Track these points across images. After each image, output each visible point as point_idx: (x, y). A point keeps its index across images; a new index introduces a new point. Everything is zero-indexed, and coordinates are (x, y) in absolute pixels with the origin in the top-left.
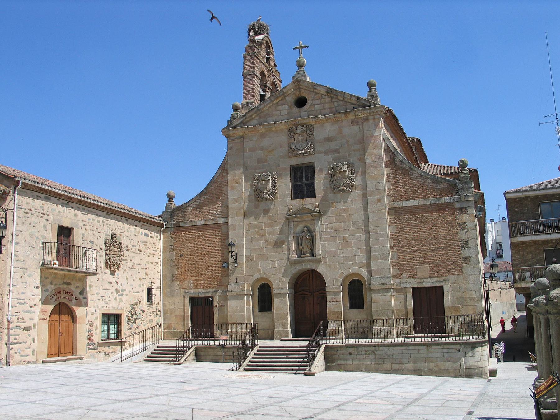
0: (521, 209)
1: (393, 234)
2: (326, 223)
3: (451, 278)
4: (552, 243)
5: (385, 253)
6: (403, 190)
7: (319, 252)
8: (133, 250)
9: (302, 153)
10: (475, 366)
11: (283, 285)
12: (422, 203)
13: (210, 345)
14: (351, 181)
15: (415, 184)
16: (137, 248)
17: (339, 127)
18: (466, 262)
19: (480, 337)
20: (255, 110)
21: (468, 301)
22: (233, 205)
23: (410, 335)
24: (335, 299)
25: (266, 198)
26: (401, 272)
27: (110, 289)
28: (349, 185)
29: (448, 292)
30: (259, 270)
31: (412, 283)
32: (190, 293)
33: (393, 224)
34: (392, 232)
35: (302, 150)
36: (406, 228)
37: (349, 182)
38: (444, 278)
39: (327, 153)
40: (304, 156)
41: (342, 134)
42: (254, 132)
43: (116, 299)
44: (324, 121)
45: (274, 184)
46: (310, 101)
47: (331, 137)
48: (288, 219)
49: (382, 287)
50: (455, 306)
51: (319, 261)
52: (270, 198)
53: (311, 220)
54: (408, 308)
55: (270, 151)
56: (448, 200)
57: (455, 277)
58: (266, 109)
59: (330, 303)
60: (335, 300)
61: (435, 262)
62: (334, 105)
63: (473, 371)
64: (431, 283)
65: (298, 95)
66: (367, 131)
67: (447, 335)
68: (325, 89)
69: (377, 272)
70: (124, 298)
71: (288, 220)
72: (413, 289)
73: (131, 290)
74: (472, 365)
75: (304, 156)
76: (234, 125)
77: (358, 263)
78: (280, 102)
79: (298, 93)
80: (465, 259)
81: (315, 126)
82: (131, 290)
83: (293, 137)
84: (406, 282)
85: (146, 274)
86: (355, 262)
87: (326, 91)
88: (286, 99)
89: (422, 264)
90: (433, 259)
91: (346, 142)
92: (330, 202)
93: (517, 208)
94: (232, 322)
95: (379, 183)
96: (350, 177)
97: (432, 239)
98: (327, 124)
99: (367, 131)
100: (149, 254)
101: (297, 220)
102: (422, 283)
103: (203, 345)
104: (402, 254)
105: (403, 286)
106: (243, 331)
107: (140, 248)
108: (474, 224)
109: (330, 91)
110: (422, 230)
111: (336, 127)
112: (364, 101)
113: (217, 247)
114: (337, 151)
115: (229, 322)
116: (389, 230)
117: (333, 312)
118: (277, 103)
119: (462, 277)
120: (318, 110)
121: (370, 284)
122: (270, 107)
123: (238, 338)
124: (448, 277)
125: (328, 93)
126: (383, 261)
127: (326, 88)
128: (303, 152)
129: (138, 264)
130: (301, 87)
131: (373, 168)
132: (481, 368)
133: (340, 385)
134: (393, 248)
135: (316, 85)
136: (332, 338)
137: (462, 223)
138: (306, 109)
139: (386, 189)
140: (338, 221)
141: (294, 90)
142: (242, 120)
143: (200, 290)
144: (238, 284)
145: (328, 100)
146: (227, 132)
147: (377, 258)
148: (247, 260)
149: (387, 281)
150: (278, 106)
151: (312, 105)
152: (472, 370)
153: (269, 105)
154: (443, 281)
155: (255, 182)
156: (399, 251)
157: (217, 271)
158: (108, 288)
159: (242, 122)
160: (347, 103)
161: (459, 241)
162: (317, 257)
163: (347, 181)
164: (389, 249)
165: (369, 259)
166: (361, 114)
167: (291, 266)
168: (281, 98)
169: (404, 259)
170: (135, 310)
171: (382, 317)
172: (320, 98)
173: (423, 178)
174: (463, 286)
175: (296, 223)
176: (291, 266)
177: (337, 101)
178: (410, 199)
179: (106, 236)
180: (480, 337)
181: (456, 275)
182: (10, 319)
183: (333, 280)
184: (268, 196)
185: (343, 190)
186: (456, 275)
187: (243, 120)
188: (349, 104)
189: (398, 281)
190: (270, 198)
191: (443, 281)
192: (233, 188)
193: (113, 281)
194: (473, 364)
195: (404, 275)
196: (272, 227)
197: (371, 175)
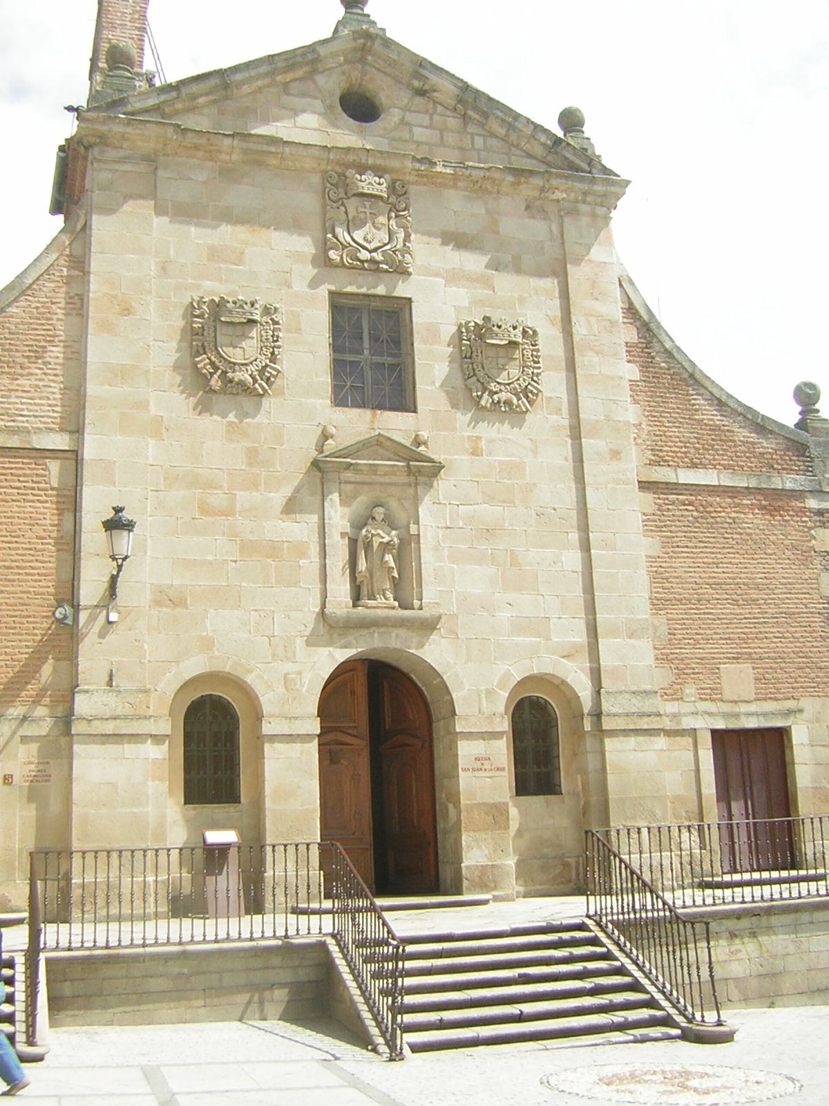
1: (653, 562)
2: (455, 503)
5: (639, 617)
7: (432, 596)
9: (372, 261)
11: (300, 704)
12: (726, 480)
13: (772, 900)
14: (533, 380)
15: (706, 425)
17: (487, 211)
20: (215, 81)
22: (107, 387)
23: (710, 879)
24: (486, 760)
25: (241, 383)
26: (680, 681)
28: (525, 391)
30: (207, 644)
33: (652, 531)
34: (650, 557)
35: (375, 250)
36: (687, 547)
37: (524, 380)
38: (791, 704)
40: (378, 270)
41: (497, 233)
42: (200, 154)
44: (447, 182)
45: (274, 341)
46: (396, 110)
47: (465, 234)
48: (320, 469)
49: (635, 724)
50: (821, 788)
51: (428, 626)
52: (257, 386)
53: (404, 484)
54: (704, 791)
56: (790, 485)
58: (246, 89)
59: (469, 773)
60: (487, 765)
62: (473, 143)
64: (761, 718)
65: (354, 81)
66: (576, 243)
67: (717, 882)
68: (455, 86)
71: (319, 474)
72: (715, 733)
75: (378, 270)
76: (129, 108)
77: (557, 642)
78: (295, 87)
79: (356, 75)
81: (413, 189)
83: (343, 204)
84: (693, 710)
86: (548, 639)
87: (457, 91)
88: (315, 82)
91: (510, 259)
94: (87, 847)
95: (615, 402)
96: (528, 367)
97: (757, 587)
98: (452, 192)
99: (576, 243)
101: (353, 480)
102: (737, 716)
103: (95, 947)
104: (679, 624)
105: (688, 723)
106: (137, 882)
109: (469, 98)
110: (730, 558)
111: (479, 209)
112: (575, 154)
113: (21, 540)
115: (76, 845)
116: (644, 546)
117: (479, 804)
118: (286, 85)
120: (426, 144)
121: (597, 715)
122: (260, 88)
123: (114, 911)
125: (460, 101)
126: (633, 641)
127: (461, 85)
128: (378, 256)
130: (369, 58)
131: (594, 355)
135: (428, 66)
136: (306, 906)
137: (825, 552)
138: (385, 129)
141: (347, 61)
142: (163, 98)
144: (119, 691)
145: (453, 122)
146: (104, 123)
147: (615, 633)
150: (289, 94)
151: (403, 122)
153: (260, 83)
154: (790, 712)
155: (199, 323)
156: (671, 613)
157: (20, 634)
159: (156, 109)
160: (513, 149)
161: (821, 601)
162: (425, 613)
163: (518, 379)
165: (593, 630)
166: (562, 190)
167: (331, 636)
168: (300, 73)
169: (684, 639)
171: (637, 822)
172: (431, 111)
173: (726, 411)
175: (349, 487)
176: (331, 636)
177: (484, 136)
178: (694, 466)
181: (819, 696)
182: (30, 763)
183: (479, 695)
184: (250, 380)
185: (508, 403)
186: (819, 696)
187: (163, 102)
188: (518, 152)
190: (257, 386)
191: (790, 712)
192: (107, 327)
195: (687, 691)
196: (257, 490)
197: (591, 375)
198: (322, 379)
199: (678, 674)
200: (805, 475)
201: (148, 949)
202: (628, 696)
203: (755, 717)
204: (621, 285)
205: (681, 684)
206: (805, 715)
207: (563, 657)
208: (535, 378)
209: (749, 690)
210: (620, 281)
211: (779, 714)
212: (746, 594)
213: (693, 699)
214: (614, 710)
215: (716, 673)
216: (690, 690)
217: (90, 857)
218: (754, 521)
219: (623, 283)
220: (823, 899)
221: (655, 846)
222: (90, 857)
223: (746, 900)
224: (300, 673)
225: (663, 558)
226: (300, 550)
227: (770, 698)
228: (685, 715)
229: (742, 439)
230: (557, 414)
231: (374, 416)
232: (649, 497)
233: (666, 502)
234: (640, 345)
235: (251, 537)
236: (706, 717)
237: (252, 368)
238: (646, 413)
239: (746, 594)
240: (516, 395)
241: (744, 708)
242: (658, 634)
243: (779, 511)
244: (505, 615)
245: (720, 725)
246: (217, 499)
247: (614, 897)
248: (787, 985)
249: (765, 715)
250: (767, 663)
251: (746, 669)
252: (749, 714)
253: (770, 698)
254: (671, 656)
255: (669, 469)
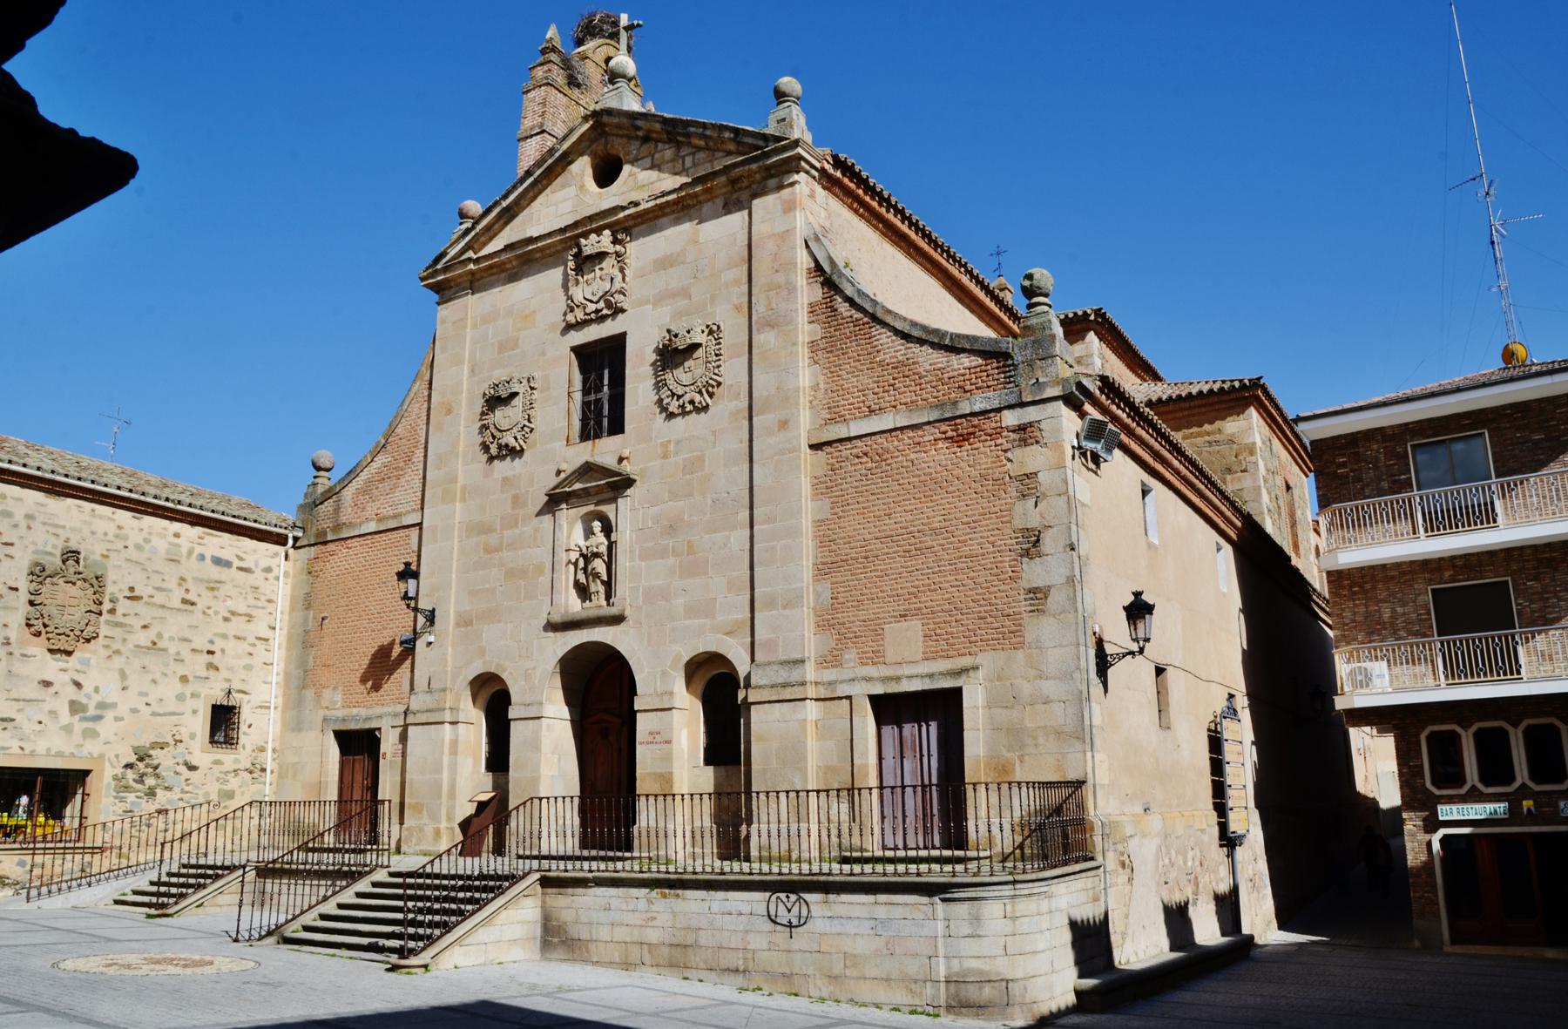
0: (1356, 467)
3: (987, 660)
4: (1454, 566)
5: (794, 586)
6: (853, 387)
8: (159, 598)
10: (981, 972)
16: (178, 594)
18: (1034, 605)
19: (1036, 866)
21: (1041, 740)
26: (840, 646)
27: (44, 701)
29: (978, 708)
31: (868, 680)
32: (336, 720)
39: (659, 300)
43: (68, 729)
47: (672, 255)
55: (526, 317)
57: (1001, 655)
59: (643, 746)
60: (658, 738)
61: (939, 608)
63: (972, 993)
69: (772, 645)
70: (107, 728)
73: (142, 707)
74: (970, 971)
80: (1032, 595)
82: (142, 707)
85: (211, 666)
89: (901, 616)
90: (932, 598)
92: (659, 441)
93: (1343, 465)
100: (228, 615)
102: (898, 679)
103: (685, 872)
105: (843, 690)
107: (191, 597)
108: (1063, 477)
114: (685, 293)
116: (808, 509)
119: (1020, 654)
124: (979, 660)
129: (180, 639)
132: (1007, 981)
133: (697, 1008)
134: (823, 570)
139: (804, 388)
140: (674, 496)
143: (355, 711)
148: (458, 625)
149: (795, 676)
152: (970, 987)
158: (32, 696)
164: (807, 573)
170: (155, 762)
174: (1026, 688)
179: (36, 556)
180: (1036, 866)
189: (829, 675)
193: (61, 680)
194: (974, 964)
198: (561, 425)
199: (839, 640)
200: (1005, 388)
201: (593, 874)
202: (775, 667)
203: (919, 679)
204: (807, 246)
205: (842, 649)
206: (980, 673)
207: (727, 634)
208: (716, 371)
209: (917, 647)
210: (806, 241)
211: (948, 674)
212: (920, 542)
213: (852, 664)
214: (762, 682)
215: (880, 635)
216: (850, 656)
217: (652, 799)
218: (939, 456)
219: (810, 244)
220: (805, 878)
221: (793, 818)
222: (652, 799)
223: (834, 872)
224: (534, 669)
225: (831, 520)
226: (539, 570)
227: (941, 657)
228: (841, 682)
229: (928, 368)
230: (736, 399)
231: (594, 444)
232: (821, 455)
233: (840, 459)
234: (824, 301)
235: (512, 565)
236: (863, 682)
237: (515, 430)
238: (825, 371)
239: (920, 542)
240: (700, 392)
241: (907, 670)
242: (820, 601)
243: (967, 440)
244: (680, 602)
245: (879, 690)
246: (493, 539)
247: (506, 859)
248: (694, 958)
249: (931, 676)
250: (939, 617)
251: (915, 627)
252: (910, 677)
253: (941, 657)
254: (832, 622)
255: (839, 425)
